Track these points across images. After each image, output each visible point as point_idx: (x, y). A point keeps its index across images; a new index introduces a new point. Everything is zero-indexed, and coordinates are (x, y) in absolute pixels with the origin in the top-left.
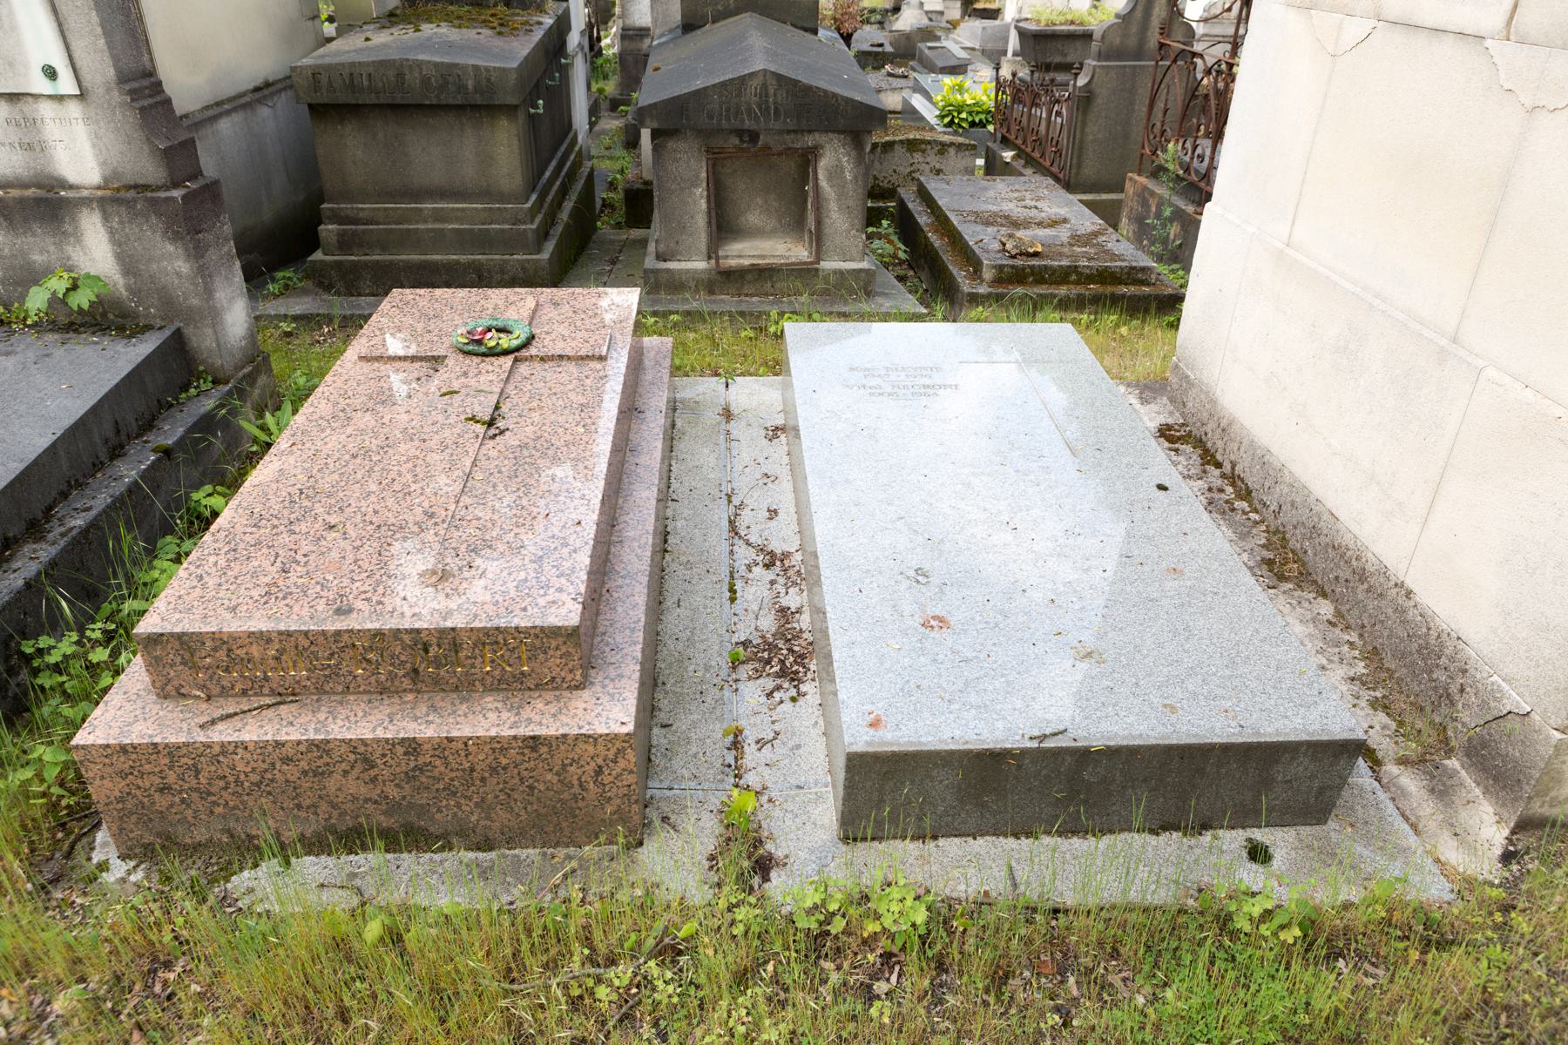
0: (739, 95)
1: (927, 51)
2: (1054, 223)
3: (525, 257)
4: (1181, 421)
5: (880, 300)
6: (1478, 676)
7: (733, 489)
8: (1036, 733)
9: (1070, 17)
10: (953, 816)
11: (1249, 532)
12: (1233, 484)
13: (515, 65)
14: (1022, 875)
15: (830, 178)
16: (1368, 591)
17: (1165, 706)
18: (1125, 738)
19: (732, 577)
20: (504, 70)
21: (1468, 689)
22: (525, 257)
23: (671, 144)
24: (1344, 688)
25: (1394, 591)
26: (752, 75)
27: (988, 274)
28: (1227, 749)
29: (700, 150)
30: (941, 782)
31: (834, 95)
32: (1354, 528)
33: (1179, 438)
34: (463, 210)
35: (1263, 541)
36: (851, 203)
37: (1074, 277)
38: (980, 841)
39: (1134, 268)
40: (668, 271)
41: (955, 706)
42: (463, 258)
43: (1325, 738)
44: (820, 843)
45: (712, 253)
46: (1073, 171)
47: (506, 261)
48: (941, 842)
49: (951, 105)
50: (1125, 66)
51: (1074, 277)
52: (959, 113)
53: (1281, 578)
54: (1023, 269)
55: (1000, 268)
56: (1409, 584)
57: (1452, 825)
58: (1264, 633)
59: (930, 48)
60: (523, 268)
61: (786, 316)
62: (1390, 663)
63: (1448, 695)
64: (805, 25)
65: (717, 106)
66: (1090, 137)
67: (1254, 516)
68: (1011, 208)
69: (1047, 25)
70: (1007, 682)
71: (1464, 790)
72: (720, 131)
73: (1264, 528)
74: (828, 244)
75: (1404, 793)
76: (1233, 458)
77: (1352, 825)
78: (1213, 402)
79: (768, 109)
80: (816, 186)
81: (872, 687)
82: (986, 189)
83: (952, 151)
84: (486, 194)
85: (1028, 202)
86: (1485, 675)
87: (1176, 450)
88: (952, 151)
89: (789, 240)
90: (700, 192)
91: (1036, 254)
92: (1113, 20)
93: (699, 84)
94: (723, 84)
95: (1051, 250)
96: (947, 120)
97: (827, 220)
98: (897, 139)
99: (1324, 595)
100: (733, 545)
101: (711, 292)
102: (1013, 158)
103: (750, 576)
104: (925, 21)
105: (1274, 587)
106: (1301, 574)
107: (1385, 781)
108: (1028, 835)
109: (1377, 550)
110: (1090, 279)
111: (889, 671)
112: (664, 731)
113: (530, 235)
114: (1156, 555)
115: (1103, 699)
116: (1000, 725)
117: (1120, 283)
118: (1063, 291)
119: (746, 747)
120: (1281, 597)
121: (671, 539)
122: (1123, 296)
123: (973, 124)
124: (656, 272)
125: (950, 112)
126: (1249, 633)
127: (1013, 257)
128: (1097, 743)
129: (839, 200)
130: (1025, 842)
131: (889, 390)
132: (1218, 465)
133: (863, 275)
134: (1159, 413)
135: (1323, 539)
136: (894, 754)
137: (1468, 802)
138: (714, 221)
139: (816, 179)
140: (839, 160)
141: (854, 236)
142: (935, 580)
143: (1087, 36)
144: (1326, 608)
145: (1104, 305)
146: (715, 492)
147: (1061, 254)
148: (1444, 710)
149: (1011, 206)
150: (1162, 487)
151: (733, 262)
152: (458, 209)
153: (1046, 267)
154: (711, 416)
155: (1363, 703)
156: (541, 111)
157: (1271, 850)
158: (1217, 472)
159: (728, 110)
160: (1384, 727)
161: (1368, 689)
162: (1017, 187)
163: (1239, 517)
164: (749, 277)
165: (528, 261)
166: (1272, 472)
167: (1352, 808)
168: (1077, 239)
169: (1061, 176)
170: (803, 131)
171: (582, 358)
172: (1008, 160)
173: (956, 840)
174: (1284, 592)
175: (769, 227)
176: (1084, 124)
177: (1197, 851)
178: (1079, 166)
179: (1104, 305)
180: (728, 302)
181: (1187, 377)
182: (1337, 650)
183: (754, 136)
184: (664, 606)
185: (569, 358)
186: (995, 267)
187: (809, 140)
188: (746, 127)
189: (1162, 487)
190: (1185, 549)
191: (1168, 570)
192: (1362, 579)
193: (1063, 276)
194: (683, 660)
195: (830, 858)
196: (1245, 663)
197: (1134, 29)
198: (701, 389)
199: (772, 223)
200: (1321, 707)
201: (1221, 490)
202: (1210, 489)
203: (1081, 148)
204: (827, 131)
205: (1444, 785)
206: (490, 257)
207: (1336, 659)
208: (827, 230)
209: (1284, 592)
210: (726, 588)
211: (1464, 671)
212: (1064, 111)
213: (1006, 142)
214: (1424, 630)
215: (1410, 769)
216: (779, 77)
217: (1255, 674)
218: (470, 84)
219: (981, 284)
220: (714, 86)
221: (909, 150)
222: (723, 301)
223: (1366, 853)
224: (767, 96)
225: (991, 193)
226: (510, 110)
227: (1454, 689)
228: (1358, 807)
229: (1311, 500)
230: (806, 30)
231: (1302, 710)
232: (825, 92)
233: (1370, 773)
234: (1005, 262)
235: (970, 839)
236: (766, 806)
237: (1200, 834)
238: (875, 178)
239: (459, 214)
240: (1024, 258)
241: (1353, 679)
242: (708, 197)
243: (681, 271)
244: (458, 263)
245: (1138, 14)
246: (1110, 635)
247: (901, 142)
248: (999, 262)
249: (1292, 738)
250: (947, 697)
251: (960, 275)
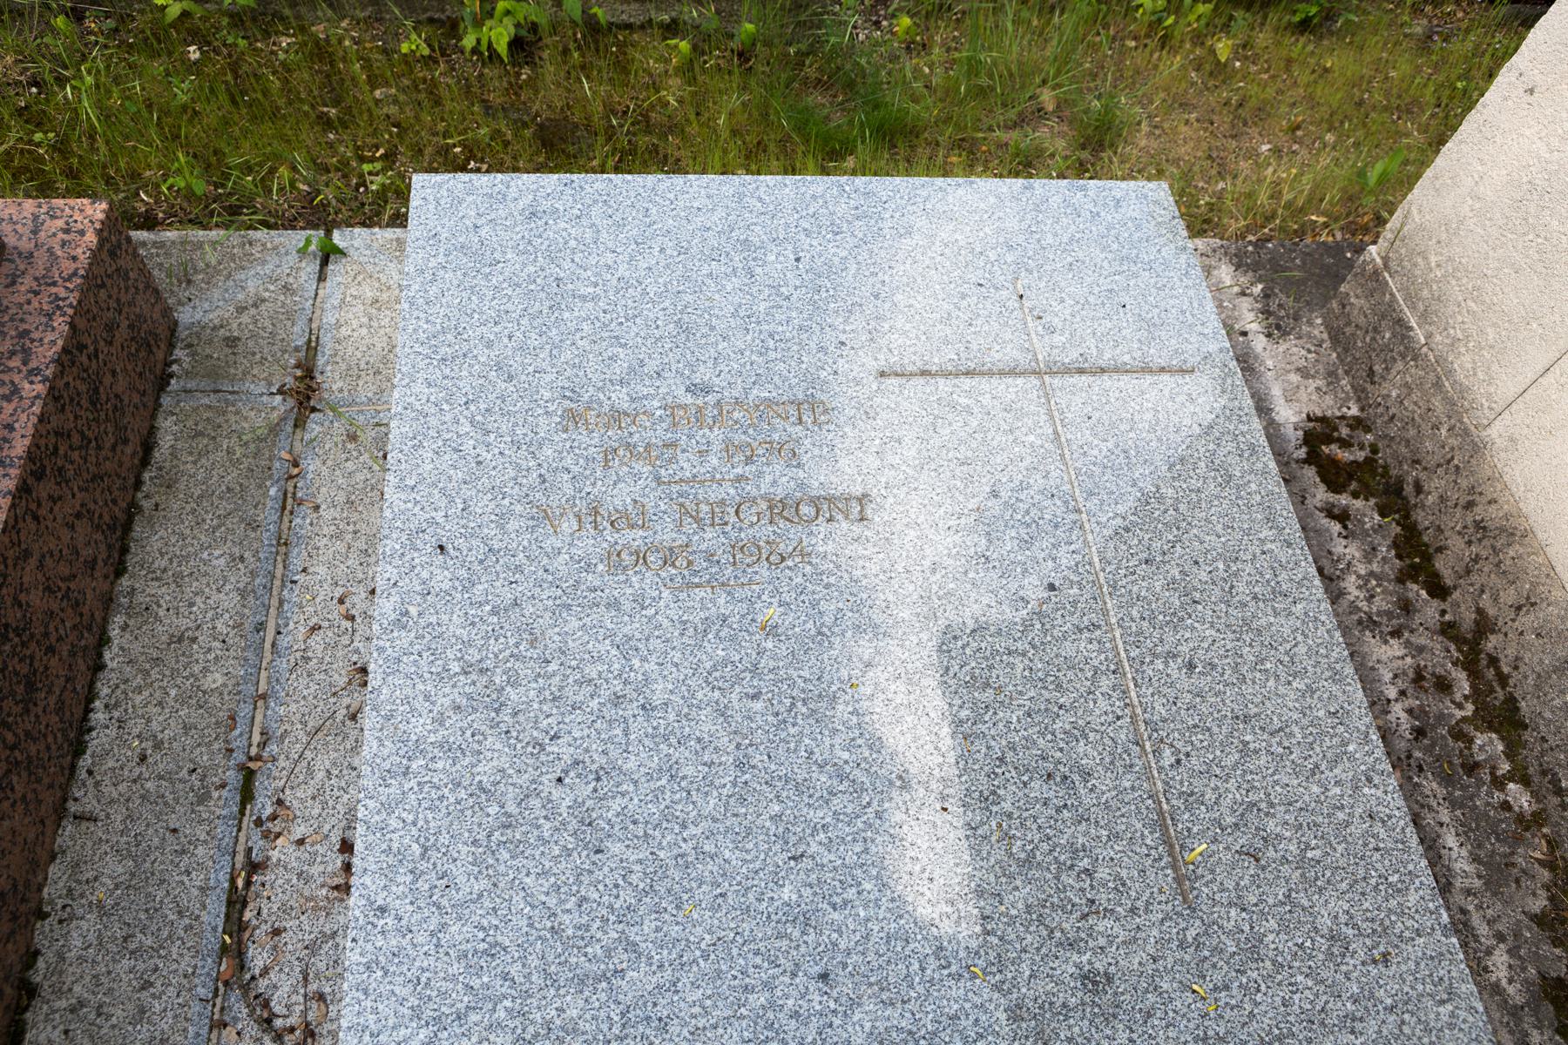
87: (1342, 517)
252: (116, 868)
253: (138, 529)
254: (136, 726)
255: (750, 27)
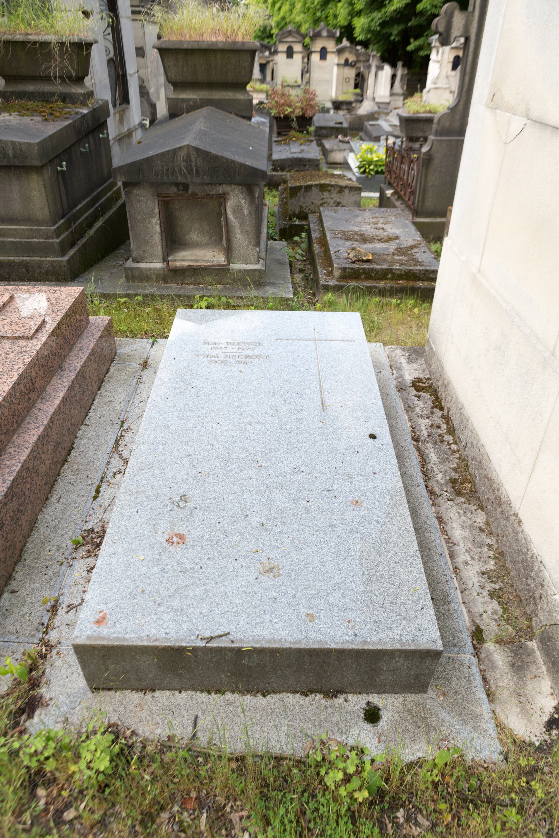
0: (173, 161)
1: (369, 127)
2: (389, 239)
3: (55, 259)
4: (428, 376)
5: (267, 288)
6: (549, 592)
7: (127, 417)
8: (207, 634)
9: (428, 108)
10: (161, 679)
11: (447, 459)
12: (447, 423)
13: (37, 140)
14: (204, 722)
15: (234, 213)
16: (502, 513)
17: (307, 615)
18: (269, 641)
19: (102, 481)
20: (29, 144)
21: (543, 598)
22: (55, 259)
23: (135, 191)
24: (476, 580)
25: (514, 518)
26: (180, 148)
27: (336, 273)
28: (341, 653)
29: (153, 195)
30: (144, 662)
31: (233, 161)
32: (497, 469)
33: (423, 388)
34: (15, 229)
35: (455, 465)
36: (248, 229)
37: (390, 276)
38: (184, 694)
39: (428, 271)
40: (139, 268)
41: (162, 609)
42: (16, 259)
43: (412, 648)
44: (77, 690)
45: (165, 260)
46: (420, 204)
47: (42, 261)
48: (157, 694)
49: (364, 161)
50: (452, 140)
51: (390, 276)
52: (369, 166)
53: (459, 494)
54: (358, 270)
55: (344, 269)
56: (521, 516)
57: (519, 695)
58: (401, 555)
59: (371, 125)
60: (52, 266)
61: (205, 298)
62: (509, 566)
63: (534, 598)
64: (244, 114)
65: (160, 168)
66: (430, 184)
67: (454, 447)
68: (368, 229)
69: (414, 113)
70: (205, 590)
71: (535, 667)
72: (164, 183)
73: (457, 456)
74: (236, 254)
75: (493, 666)
76: (449, 406)
77: (444, 694)
78: (442, 367)
79: (192, 170)
80: (226, 218)
81: (111, 590)
82: (357, 216)
83: (347, 191)
84: (28, 220)
85: (380, 225)
86: (552, 593)
87: (419, 397)
88: (347, 191)
89: (216, 250)
90: (155, 220)
91: (368, 261)
92: (446, 111)
93: (151, 153)
94: (163, 154)
95: (378, 257)
96: (362, 170)
97: (234, 239)
98: (314, 183)
99: (482, 508)
100: (111, 458)
101: (166, 282)
102: (392, 194)
103: (113, 481)
104: (376, 108)
105: (451, 500)
106: (471, 491)
107: (483, 655)
108: (218, 691)
109: (507, 488)
110: (400, 277)
111: (129, 577)
112: (10, 596)
113: (56, 246)
114: (348, 489)
115: (266, 607)
116: (185, 626)
117: (419, 280)
118: (381, 284)
119: (60, 610)
120: (454, 508)
121: (73, 453)
122: (420, 288)
123: (377, 172)
124: (132, 269)
125: (364, 165)
126: (390, 556)
127: (354, 262)
128: (247, 646)
129: (241, 226)
130: (214, 696)
131: (222, 358)
132: (442, 409)
133: (257, 273)
134: (416, 370)
135: (485, 473)
136: (103, 647)
137: (535, 677)
138: (164, 239)
139: (226, 214)
140: (239, 202)
141: (252, 249)
142: (190, 505)
143: (429, 121)
144: (480, 518)
145: (406, 293)
146: (115, 420)
147: (384, 261)
148: (532, 607)
149: (368, 227)
150: (373, 437)
151: (178, 264)
152: (12, 229)
153: (372, 269)
154: (134, 365)
155: (485, 593)
156: (65, 169)
157: (381, 713)
158: (440, 413)
159: (167, 170)
160: (495, 613)
161: (492, 582)
162: (377, 215)
163: (444, 447)
164: (188, 273)
165: (55, 261)
166: (465, 421)
167: (450, 680)
168: (400, 251)
169: (412, 207)
170: (215, 184)
171: (16, 338)
172: (389, 196)
173: (167, 693)
174: (457, 504)
175: (204, 242)
176: (426, 176)
177: (330, 711)
178: (423, 201)
179: (406, 293)
180: (173, 288)
181: (432, 349)
182: (479, 550)
183: (186, 187)
184: (49, 501)
185: (8, 338)
186: (340, 269)
187: (221, 189)
188: (179, 181)
189: (373, 437)
190: (370, 486)
191: (352, 503)
192: (500, 505)
193: (383, 275)
194: (46, 540)
195: (78, 703)
196: (378, 581)
197: (458, 117)
198: (135, 347)
199: (205, 240)
200: (419, 621)
201: (439, 427)
202: (432, 426)
203: (424, 191)
204: (231, 184)
205: (522, 661)
206: (33, 258)
207: (476, 557)
208: (235, 245)
209: (457, 504)
210: (95, 488)
211: (543, 586)
212: (415, 167)
213: (390, 185)
214: (526, 549)
215: (502, 648)
216: (197, 150)
217: (381, 590)
218: (11, 153)
219: (332, 279)
220: (157, 155)
221: (320, 190)
222: (171, 287)
223: (448, 718)
224: (190, 162)
225: (360, 219)
226: (39, 169)
227: (537, 595)
228: (454, 679)
229: (480, 444)
230: (244, 117)
231: (404, 622)
232: (227, 159)
233: (472, 651)
234: (347, 266)
235: (177, 693)
236: (54, 657)
237: (336, 697)
238: (301, 207)
239: (13, 232)
240: (360, 263)
241: (483, 573)
242: (160, 223)
243: (146, 269)
244: (13, 262)
245: (461, 107)
246: (291, 554)
247: (316, 185)
248: (344, 266)
249: (389, 647)
250: (159, 600)
251: (322, 272)
252: (92, 433)
253: (104, 384)
254: (99, 413)
255: (271, 304)
